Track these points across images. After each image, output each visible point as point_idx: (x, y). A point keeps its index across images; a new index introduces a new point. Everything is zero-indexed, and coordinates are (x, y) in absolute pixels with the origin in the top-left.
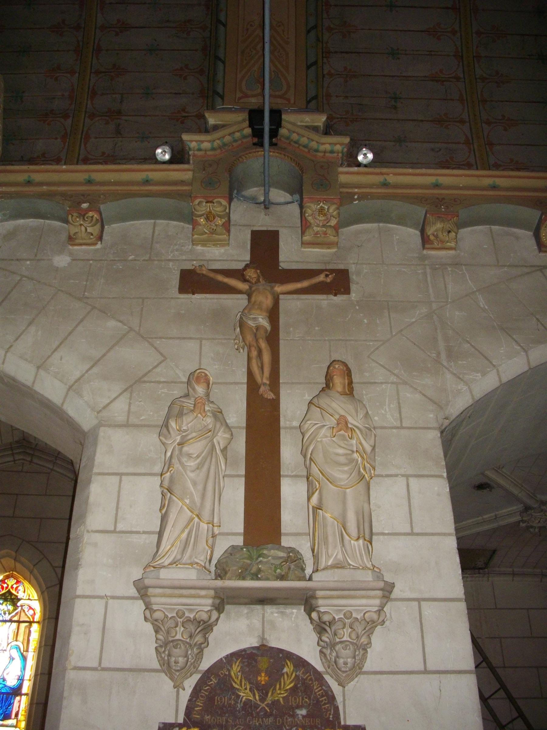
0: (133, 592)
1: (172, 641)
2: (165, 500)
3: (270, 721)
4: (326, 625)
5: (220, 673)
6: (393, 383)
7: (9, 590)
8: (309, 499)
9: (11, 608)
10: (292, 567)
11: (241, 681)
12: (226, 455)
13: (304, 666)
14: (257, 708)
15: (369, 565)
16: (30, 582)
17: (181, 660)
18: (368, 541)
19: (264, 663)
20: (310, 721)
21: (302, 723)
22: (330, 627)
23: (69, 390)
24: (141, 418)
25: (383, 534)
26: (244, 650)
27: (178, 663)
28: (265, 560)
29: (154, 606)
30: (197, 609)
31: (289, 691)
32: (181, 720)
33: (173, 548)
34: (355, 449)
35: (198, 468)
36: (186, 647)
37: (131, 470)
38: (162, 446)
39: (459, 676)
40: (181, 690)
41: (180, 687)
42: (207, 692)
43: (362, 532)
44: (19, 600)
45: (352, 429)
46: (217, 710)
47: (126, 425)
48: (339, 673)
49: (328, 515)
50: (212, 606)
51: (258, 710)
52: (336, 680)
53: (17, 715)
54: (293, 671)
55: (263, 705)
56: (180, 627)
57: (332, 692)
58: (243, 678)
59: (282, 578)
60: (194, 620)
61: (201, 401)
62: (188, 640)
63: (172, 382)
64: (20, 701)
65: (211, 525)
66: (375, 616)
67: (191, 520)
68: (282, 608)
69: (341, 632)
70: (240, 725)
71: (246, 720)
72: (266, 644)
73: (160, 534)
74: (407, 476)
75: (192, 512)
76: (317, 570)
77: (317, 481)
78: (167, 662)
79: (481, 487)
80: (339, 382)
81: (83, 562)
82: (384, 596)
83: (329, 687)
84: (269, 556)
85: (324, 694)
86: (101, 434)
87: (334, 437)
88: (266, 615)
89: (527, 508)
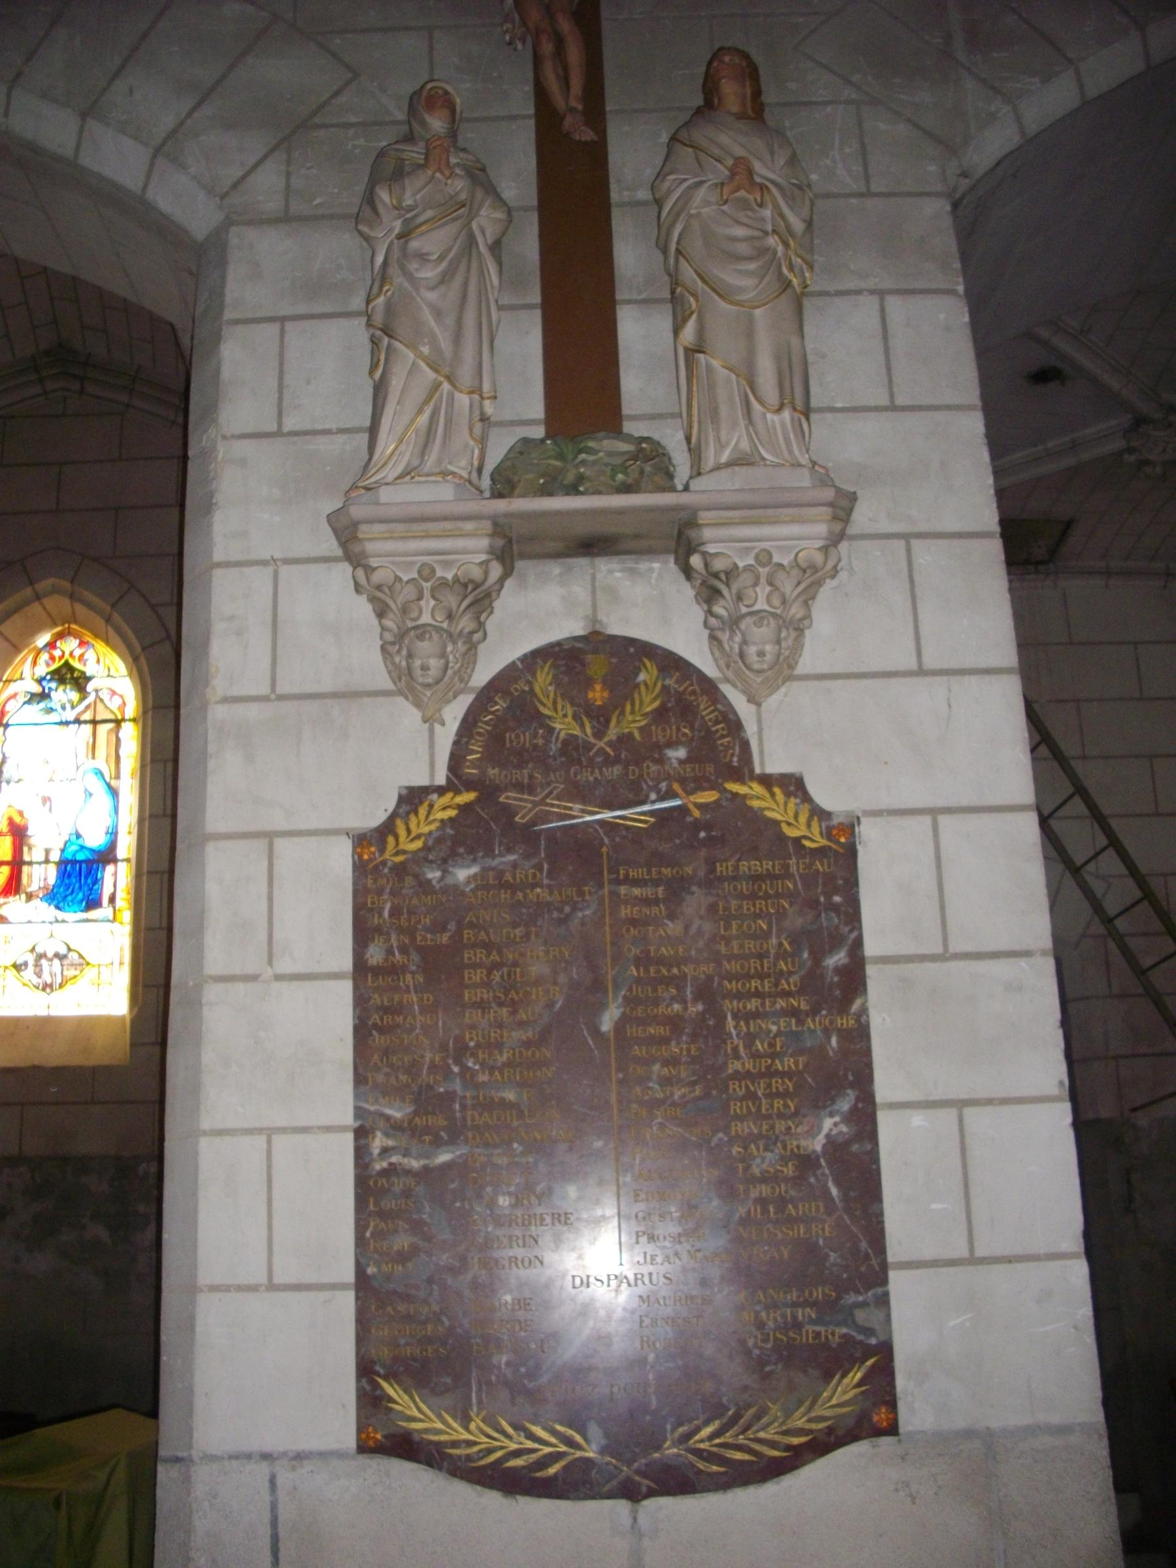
0: (329, 545)
1: (413, 628)
2: (379, 350)
3: (616, 772)
4: (720, 580)
5: (512, 690)
6: (848, 102)
7: (67, 664)
8: (676, 332)
9: (74, 696)
10: (648, 468)
11: (555, 703)
12: (500, 257)
13: (677, 669)
14: (590, 750)
15: (804, 460)
16: (107, 642)
17: (435, 664)
18: (802, 413)
19: (597, 666)
20: (693, 769)
21: (679, 773)
22: (728, 585)
23: (154, 156)
24: (315, 203)
25: (832, 410)
26: (559, 644)
27: (428, 669)
28: (592, 458)
29: (371, 560)
30: (460, 560)
31: (650, 716)
32: (441, 779)
33: (403, 447)
34: (769, 228)
35: (442, 282)
36: (441, 636)
37: (302, 309)
38: (365, 244)
39: (987, 678)
40: (437, 726)
41: (435, 721)
42: (489, 725)
43: (787, 391)
44: (89, 679)
45: (762, 187)
46: (512, 758)
47: (285, 218)
48: (748, 677)
49: (715, 363)
50: (488, 553)
51: (591, 754)
52: (744, 692)
53: (112, 899)
54: (657, 678)
55: (601, 744)
56: (428, 601)
57: (735, 714)
58: (559, 695)
59: (626, 489)
60: (454, 583)
61: (438, 143)
62: (445, 625)
63: (375, 124)
64: (115, 874)
65: (476, 397)
66: (819, 558)
67: (436, 387)
68: (629, 561)
69: (750, 592)
70: (557, 782)
71: (568, 772)
72: (602, 630)
73: (373, 430)
74: (881, 293)
75: (436, 371)
76: (699, 474)
77: (693, 295)
78: (406, 672)
79: (1042, 376)
80: (731, 91)
81: (219, 498)
82: (835, 518)
83: (730, 705)
84: (599, 451)
85: (720, 718)
86: (233, 240)
87: (726, 202)
88: (599, 576)
89: (1139, 422)
